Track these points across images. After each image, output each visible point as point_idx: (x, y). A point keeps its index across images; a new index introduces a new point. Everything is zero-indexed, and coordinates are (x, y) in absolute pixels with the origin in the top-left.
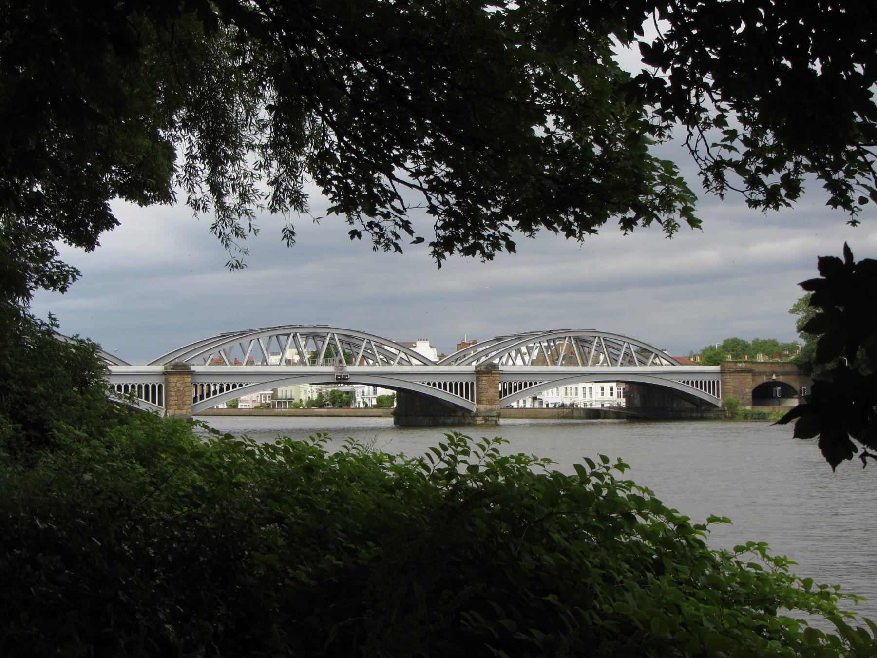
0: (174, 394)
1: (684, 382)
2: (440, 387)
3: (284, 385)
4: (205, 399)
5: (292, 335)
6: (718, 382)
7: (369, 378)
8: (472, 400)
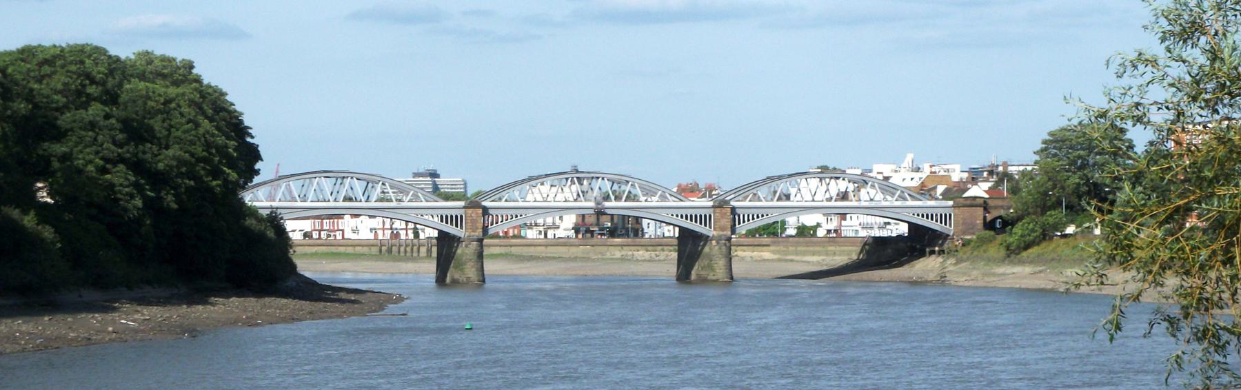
0: (469, 221)
1: (918, 215)
2: (687, 218)
3: (803, 214)
4: (494, 225)
5: (570, 179)
6: (950, 215)
7: (623, 210)
8: (710, 227)
